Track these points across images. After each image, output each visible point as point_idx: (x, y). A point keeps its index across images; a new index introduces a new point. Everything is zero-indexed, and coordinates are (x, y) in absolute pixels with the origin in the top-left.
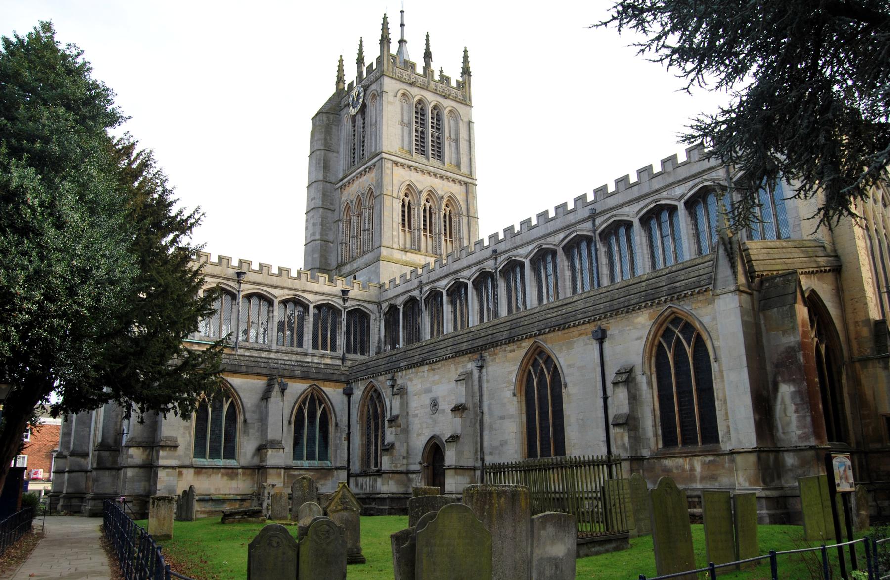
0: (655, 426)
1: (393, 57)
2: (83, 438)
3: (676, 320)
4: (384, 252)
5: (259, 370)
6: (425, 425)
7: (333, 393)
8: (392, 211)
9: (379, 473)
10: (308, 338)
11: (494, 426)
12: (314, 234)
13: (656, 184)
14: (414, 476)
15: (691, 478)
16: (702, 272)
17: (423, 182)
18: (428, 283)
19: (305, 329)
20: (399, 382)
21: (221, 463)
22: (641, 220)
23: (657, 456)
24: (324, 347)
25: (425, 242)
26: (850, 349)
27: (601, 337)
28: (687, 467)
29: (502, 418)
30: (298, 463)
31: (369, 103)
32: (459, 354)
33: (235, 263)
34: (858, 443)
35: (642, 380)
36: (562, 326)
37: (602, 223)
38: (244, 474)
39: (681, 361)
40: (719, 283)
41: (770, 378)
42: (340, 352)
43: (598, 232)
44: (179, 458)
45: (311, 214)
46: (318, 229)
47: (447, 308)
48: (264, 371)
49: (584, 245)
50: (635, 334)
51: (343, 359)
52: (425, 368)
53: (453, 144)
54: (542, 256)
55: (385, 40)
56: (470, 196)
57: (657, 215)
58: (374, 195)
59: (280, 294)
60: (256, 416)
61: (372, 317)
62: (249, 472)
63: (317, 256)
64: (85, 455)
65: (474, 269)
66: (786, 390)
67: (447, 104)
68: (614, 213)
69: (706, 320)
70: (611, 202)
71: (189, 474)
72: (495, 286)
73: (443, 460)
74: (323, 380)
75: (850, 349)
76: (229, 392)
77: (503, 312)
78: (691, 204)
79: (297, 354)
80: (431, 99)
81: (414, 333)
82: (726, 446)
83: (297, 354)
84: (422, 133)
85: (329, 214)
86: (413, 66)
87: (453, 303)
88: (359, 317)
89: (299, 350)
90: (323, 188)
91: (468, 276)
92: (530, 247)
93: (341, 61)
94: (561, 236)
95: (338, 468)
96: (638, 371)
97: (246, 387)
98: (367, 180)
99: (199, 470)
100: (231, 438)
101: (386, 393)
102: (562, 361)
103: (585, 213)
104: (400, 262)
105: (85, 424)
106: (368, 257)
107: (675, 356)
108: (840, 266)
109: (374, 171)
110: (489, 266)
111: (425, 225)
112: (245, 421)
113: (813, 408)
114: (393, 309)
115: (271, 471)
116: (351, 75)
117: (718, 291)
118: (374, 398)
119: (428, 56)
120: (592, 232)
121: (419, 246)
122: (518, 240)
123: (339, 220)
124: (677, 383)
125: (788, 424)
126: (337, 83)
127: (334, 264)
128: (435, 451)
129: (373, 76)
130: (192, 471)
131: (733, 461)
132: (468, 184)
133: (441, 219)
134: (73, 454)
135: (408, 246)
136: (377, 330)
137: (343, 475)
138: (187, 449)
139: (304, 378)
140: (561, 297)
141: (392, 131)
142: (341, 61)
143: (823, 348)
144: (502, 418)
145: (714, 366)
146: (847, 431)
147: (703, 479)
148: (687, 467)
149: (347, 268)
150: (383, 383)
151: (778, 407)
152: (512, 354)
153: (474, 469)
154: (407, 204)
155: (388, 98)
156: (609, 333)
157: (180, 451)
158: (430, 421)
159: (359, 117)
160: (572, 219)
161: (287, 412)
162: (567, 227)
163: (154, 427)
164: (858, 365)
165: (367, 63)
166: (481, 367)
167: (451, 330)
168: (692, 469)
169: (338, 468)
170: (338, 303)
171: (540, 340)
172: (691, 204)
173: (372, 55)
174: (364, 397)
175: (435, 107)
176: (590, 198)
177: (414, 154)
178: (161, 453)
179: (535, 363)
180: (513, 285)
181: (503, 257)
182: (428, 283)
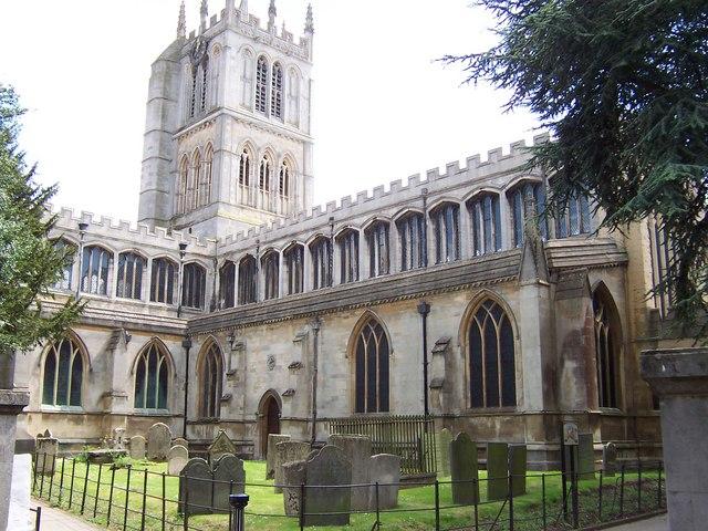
0: (465, 390)
3: (489, 302)
4: (222, 210)
6: (262, 380)
7: (173, 346)
8: (230, 168)
9: (216, 422)
11: (327, 384)
12: (150, 183)
13: (483, 172)
14: (250, 425)
15: (492, 433)
16: (512, 263)
17: (262, 139)
18: (265, 243)
19: (143, 281)
20: (238, 339)
23: (466, 416)
24: (161, 300)
25: (262, 198)
26: (629, 333)
27: (425, 311)
28: (489, 424)
29: (334, 377)
30: (139, 410)
32: (296, 317)
33: (77, 215)
34: (628, 410)
35: (457, 351)
36: (393, 299)
37: (432, 203)
38: (89, 419)
39: (490, 338)
41: (559, 355)
42: (176, 305)
43: (429, 209)
45: (147, 164)
46: (155, 179)
47: (283, 269)
49: (415, 221)
50: (454, 310)
52: (264, 327)
53: (293, 102)
56: (308, 154)
57: (482, 201)
58: (215, 150)
61: (208, 272)
62: (93, 417)
63: (152, 206)
65: (310, 234)
66: (570, 365)
68: (444, 195)
69: (512, 304)
70: (442, 184)
72: (330, 252)
73: (279, 412)
74: (165, 333)
75: (629, 333)
76: (77, 343)
78: (511, 194)
80: (273, 56)
81: (249, 294)
82: (520, 409)
84: (263, 89)
86: (257, 21)
88: (195, 272)
89: (137, 301)
90: (161, 139)
91: (305, 240)
92: (365, 218)
94: (395, 210)
96: (454, 343)
102: (390, 329)
103: (418, 192)
104: (239, 221)
106: (206, 211)
108: (627, 261)
109: (215, 126)
110: (325, 232)
111: (262, 182)
112: (91, 370)
114: (229, 265)
115: (116, 417)
117: (523, 283)
119: (272, 10)
120: (421, 218)
121: (256, 203)
123: (176, 171)
124: (486, 354)
127: (169, 216)
128: (271, 404)
129: (216, 28)
130: (40, 415)
131: (524, 421)
135: (245, 201)
136: (212, 284)
137: (180, 422)
138: (37, 395)
140: (392, 272)
141: (233, 85)
142: (183, 7)
143: (606, 331)
144: (334, 377)
145: (516, 342)
146: (620, 399)
148: (489, 424)
149: (183, 221)
150: (222, 339)
151: (563, 380)
152: (346, 321)
153: (307, 421)
154: (245, 160)
155: (231, 53)
158: (266, 376)
159: (200, 68)
160: (405, 196)
164: (634, 345)
165: (211, 14)
166: (317, 330)
168: (493, 426)
170: (175, 257)
172: (511, 194)
174: (203, 351)
175: (276, 64)
176: (423, 178)
177: (254, 110)
179: (367, 330)
180: (347, 251)
181: (339, 225)
182: (265, 243)
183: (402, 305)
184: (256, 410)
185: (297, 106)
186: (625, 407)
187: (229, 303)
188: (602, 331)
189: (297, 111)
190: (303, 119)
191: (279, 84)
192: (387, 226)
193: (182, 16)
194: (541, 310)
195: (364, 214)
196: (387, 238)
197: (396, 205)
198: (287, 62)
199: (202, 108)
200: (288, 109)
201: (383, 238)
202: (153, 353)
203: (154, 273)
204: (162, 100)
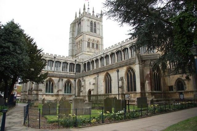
0: (126, 88)
1: (86, 12)
2: (26, 89)
5: (57, 76)
7: (72, 81)
10: (68, 70)
17: (92, 38)
20: (84, 79)
21: (51, 94)
22: (130, 48)
25: (93, 50)
27: (118, 71)
29: (101, 86)
31: (81, 22)
33: (54, 55)
36: (112, 69)
40: (136, 62)
42: (74, 73)
44: (42, 93)
47: (95, 64)
48: (59, 76)
51: (75, 74)
52: (89, 76)
54: (112, 54)
55: (84, 9)
59: (62, 61)
60: (57, 85)
63: (71, 53)
64: (26, 92)
66: (147, 82)
67: (97, 22)
71: (44, 96)
72: (104, 60)
77: (105, 65)
79: (66, 73)
80: (94, 21)
81: (89, 69)
83: (66, 73)
85: (73, 44)
87: (96, 63)
88: (79, 65)
92: (110, 52)
93: (76, 13)
94: (115, 50)
95: (73, 95)
97: (55, 80)
98: (81, 38)
99: (46, 95)
100: (52, 89)
101: (82, 81)
103: (120, 46)
104: (86, 55)
105: (26, 86)
107: (130, 75)
110: (103, 56)
112: (55, 86)
113: (195, 78)
114: (85, 64)
116: (78, 16)
117: (136, 64)
118: (79, 81)
119: (93, 12)
120: (120, 51)
122: (108, 51)
125: (147, 88)
126: (75, 17)
127: (74, 55)
129: (82, 16)
132: (102, 38)
133: (96, 45)
134: (24, 92)
136: (82, 68)
137: (74, 96)
138: (44, 91)
139: (66, 78)
141: (86, 27)
142: (76, 13)
144: (101, 86)
146: (161, 88)
147: (133, 98)
149: (77, 55)
150: (81, 79)
156: (119, 70)
157: (43, 91)
159: (79, 25)
160: (118, 47)
161: (63, 84)
162: (117, 49)
163: (38, 87)
166: (98, 76)
167: (96, 68)
169: (73, 95)
170: (74, 63)
171: (108, 72)
173: (82, 13)
175: (95, 22)
178: (39, 92)
183: (114, 70)
184: (87, 93)
185: (99, 31)
186: (162, 90)
187: (85, 71)
188: (157, 74)
189: (100, 32)
190: (101, 33)
191: (95, 26)
192: (114, 54)
193: (76, 14)
194: (140, 70)
195: (110, 52)
196: (114, 56)
197: (116, 49)
198: (97, 22)
199: (80, 33)
200: (97, 31)
201: (114, 56)
202: (68, 82)
203: (70, 67)
204: (72, 31)
